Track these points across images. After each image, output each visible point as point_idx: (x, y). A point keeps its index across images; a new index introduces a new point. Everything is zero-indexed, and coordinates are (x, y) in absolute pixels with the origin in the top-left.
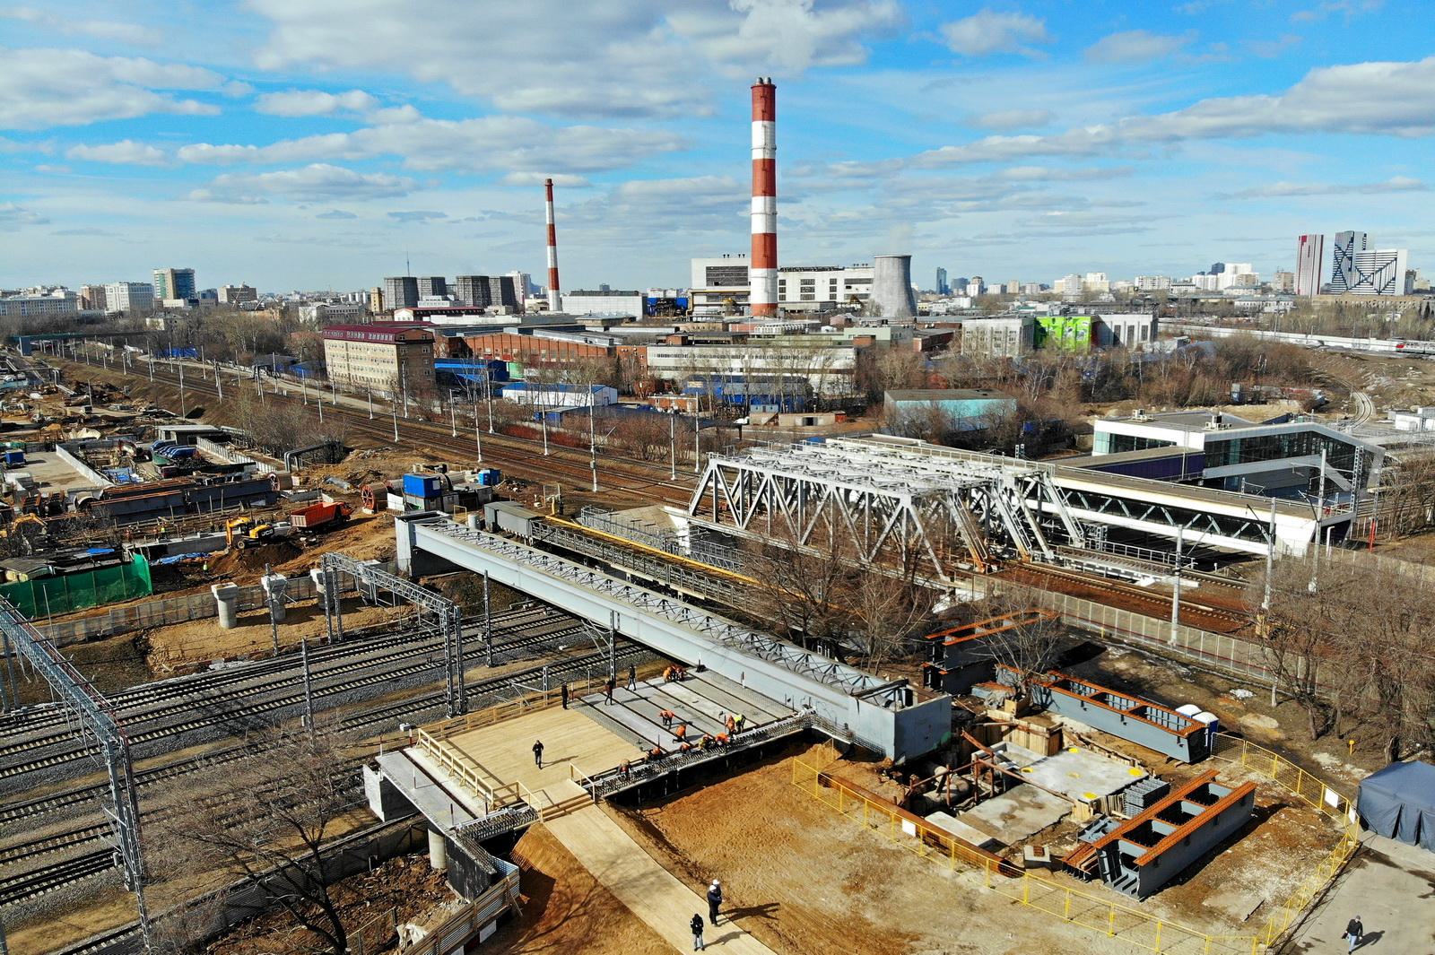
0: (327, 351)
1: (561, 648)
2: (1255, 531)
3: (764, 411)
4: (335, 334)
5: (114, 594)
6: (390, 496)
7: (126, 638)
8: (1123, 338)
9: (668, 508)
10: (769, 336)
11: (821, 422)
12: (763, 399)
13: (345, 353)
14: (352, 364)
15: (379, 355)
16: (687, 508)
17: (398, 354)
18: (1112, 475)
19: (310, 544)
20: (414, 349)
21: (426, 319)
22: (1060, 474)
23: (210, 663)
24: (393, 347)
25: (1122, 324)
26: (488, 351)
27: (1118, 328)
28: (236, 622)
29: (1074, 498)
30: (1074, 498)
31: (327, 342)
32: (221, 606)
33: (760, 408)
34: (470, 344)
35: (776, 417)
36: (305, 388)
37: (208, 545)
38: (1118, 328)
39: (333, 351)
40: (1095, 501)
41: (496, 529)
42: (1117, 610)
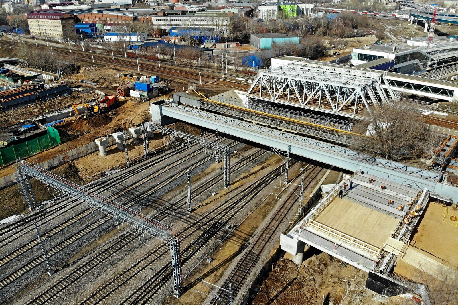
0: (29, 23)
1: (235, 152)
2: (451, 93)
3: (210, 42)
4: (33, 17)
5: (45, 145)
6: (131, 91)
7: (67, 165)
8: (305, 12)
9: (236, 91)
10: (194, 12)
11: (231, 46)
12: (210, 38)
13: (37, 24)
14: (41, 28)
15: (53, 24)
16: (247, 91)
17: (62, 24)
18: (371, 70)
19: (114, 115)
20: (68, 22)
21: (54, 8)
22: (388, 75)
23: (105, 172)
24: (60, 21)
25: (305, 8)
26: (87, 19)
27: (303, 9)
28: (108, 153)
29: (392, 83)
30: (392, 83)
31: (29, 20)
32: (101, 148)
33: (209, 41)
34: (79, 17)
35: (215, 44)
36: (23, 38)
37: (61, 116)
38: (303, 9)
39: (32, 23)
40: (401, 84)
41: (179, 103)
42: (439, 127)
